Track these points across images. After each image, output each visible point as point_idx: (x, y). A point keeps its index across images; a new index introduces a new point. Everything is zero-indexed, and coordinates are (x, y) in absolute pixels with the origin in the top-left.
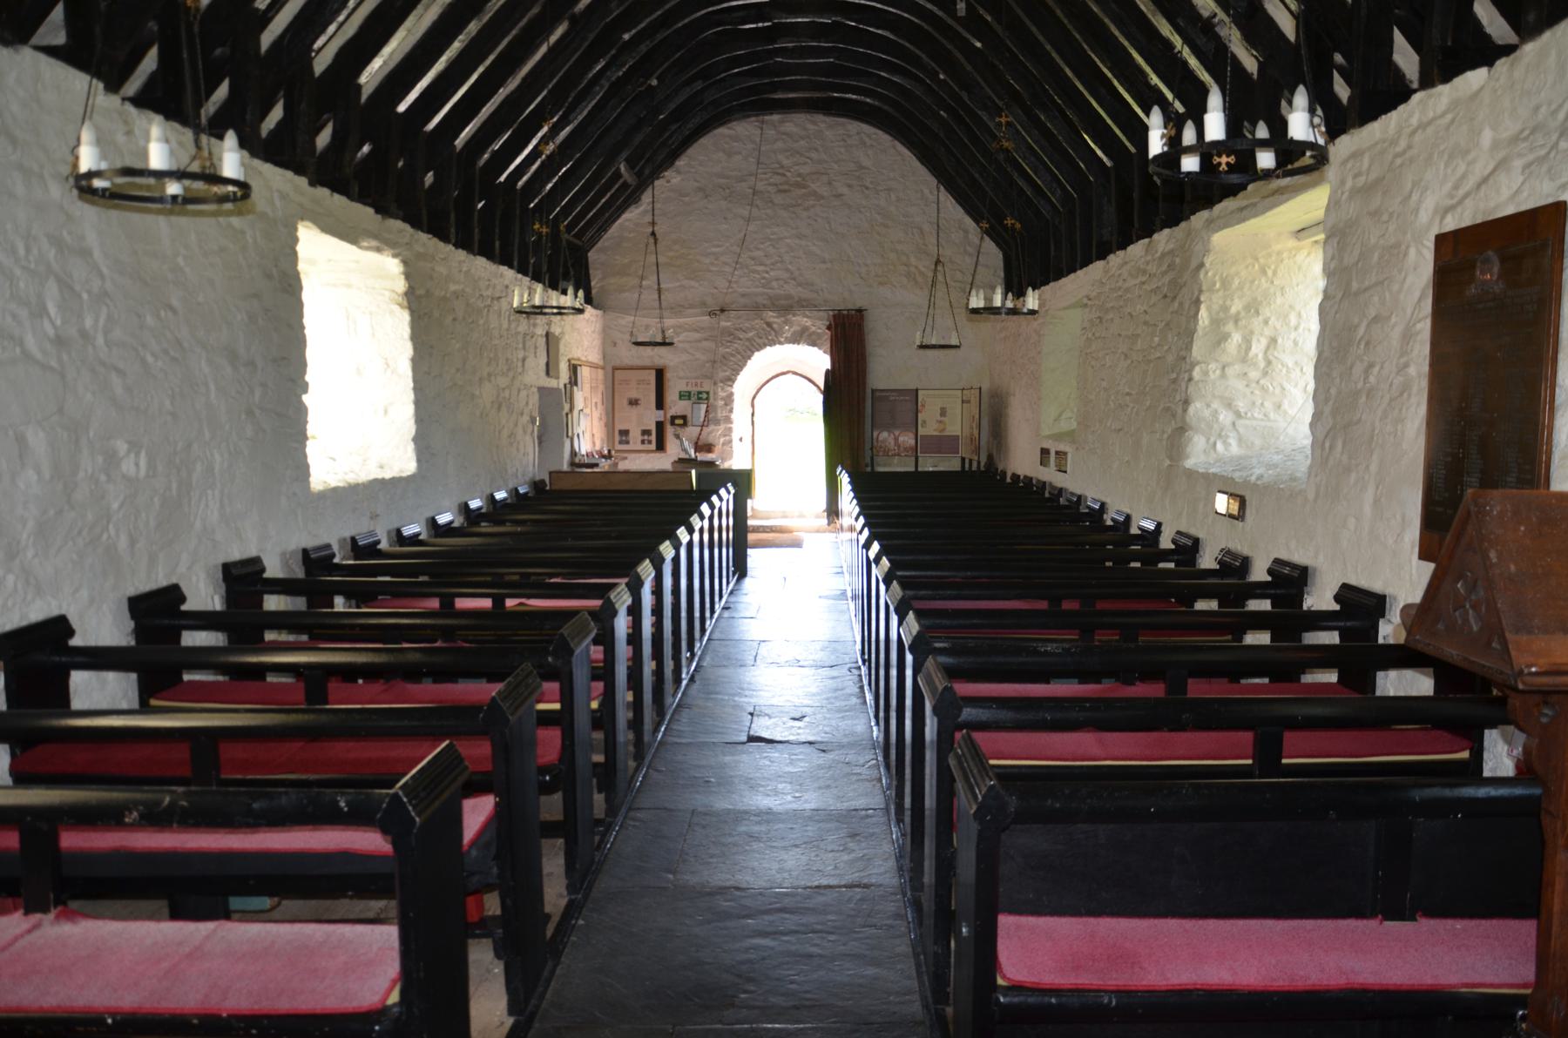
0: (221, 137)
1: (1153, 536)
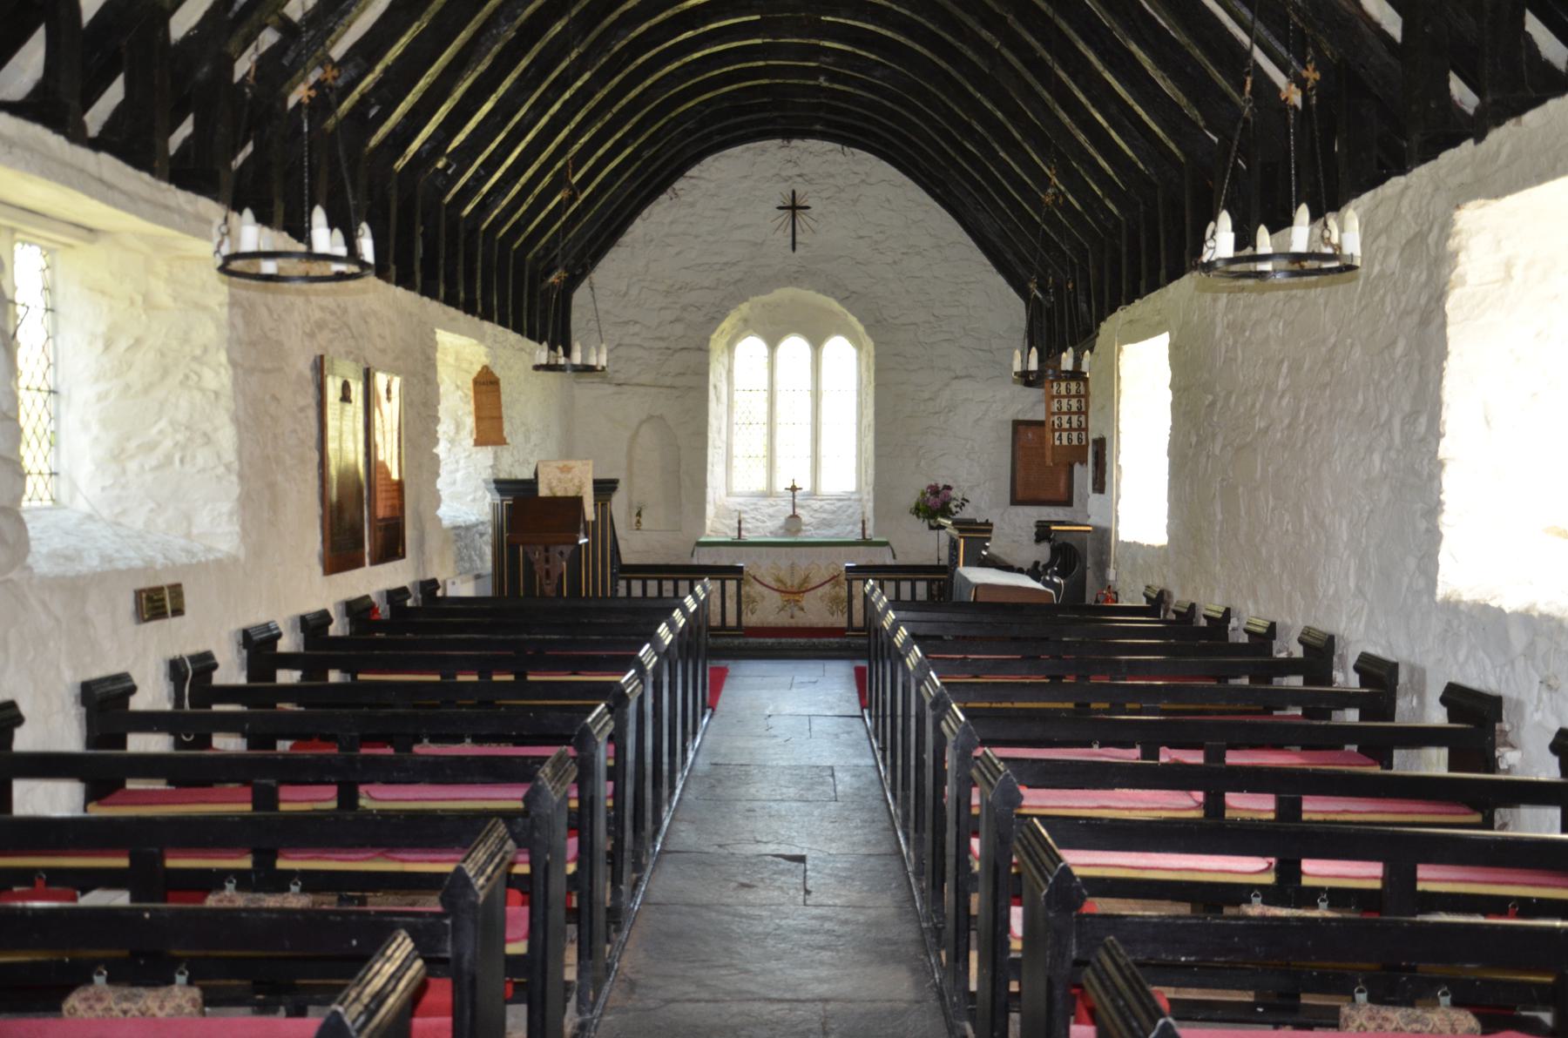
0: (241, 213)
1: (1220, 624)
